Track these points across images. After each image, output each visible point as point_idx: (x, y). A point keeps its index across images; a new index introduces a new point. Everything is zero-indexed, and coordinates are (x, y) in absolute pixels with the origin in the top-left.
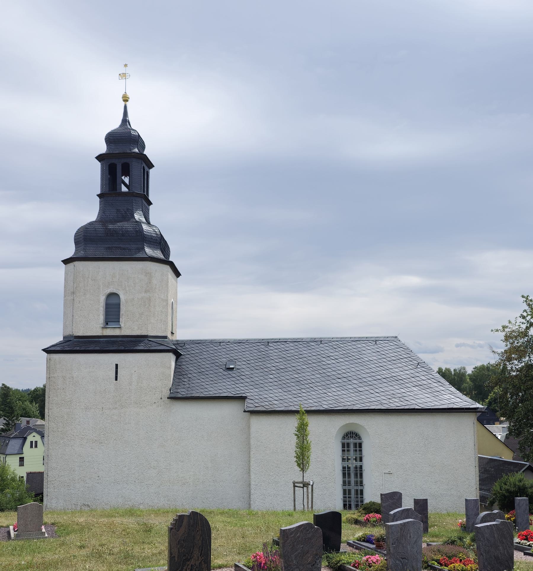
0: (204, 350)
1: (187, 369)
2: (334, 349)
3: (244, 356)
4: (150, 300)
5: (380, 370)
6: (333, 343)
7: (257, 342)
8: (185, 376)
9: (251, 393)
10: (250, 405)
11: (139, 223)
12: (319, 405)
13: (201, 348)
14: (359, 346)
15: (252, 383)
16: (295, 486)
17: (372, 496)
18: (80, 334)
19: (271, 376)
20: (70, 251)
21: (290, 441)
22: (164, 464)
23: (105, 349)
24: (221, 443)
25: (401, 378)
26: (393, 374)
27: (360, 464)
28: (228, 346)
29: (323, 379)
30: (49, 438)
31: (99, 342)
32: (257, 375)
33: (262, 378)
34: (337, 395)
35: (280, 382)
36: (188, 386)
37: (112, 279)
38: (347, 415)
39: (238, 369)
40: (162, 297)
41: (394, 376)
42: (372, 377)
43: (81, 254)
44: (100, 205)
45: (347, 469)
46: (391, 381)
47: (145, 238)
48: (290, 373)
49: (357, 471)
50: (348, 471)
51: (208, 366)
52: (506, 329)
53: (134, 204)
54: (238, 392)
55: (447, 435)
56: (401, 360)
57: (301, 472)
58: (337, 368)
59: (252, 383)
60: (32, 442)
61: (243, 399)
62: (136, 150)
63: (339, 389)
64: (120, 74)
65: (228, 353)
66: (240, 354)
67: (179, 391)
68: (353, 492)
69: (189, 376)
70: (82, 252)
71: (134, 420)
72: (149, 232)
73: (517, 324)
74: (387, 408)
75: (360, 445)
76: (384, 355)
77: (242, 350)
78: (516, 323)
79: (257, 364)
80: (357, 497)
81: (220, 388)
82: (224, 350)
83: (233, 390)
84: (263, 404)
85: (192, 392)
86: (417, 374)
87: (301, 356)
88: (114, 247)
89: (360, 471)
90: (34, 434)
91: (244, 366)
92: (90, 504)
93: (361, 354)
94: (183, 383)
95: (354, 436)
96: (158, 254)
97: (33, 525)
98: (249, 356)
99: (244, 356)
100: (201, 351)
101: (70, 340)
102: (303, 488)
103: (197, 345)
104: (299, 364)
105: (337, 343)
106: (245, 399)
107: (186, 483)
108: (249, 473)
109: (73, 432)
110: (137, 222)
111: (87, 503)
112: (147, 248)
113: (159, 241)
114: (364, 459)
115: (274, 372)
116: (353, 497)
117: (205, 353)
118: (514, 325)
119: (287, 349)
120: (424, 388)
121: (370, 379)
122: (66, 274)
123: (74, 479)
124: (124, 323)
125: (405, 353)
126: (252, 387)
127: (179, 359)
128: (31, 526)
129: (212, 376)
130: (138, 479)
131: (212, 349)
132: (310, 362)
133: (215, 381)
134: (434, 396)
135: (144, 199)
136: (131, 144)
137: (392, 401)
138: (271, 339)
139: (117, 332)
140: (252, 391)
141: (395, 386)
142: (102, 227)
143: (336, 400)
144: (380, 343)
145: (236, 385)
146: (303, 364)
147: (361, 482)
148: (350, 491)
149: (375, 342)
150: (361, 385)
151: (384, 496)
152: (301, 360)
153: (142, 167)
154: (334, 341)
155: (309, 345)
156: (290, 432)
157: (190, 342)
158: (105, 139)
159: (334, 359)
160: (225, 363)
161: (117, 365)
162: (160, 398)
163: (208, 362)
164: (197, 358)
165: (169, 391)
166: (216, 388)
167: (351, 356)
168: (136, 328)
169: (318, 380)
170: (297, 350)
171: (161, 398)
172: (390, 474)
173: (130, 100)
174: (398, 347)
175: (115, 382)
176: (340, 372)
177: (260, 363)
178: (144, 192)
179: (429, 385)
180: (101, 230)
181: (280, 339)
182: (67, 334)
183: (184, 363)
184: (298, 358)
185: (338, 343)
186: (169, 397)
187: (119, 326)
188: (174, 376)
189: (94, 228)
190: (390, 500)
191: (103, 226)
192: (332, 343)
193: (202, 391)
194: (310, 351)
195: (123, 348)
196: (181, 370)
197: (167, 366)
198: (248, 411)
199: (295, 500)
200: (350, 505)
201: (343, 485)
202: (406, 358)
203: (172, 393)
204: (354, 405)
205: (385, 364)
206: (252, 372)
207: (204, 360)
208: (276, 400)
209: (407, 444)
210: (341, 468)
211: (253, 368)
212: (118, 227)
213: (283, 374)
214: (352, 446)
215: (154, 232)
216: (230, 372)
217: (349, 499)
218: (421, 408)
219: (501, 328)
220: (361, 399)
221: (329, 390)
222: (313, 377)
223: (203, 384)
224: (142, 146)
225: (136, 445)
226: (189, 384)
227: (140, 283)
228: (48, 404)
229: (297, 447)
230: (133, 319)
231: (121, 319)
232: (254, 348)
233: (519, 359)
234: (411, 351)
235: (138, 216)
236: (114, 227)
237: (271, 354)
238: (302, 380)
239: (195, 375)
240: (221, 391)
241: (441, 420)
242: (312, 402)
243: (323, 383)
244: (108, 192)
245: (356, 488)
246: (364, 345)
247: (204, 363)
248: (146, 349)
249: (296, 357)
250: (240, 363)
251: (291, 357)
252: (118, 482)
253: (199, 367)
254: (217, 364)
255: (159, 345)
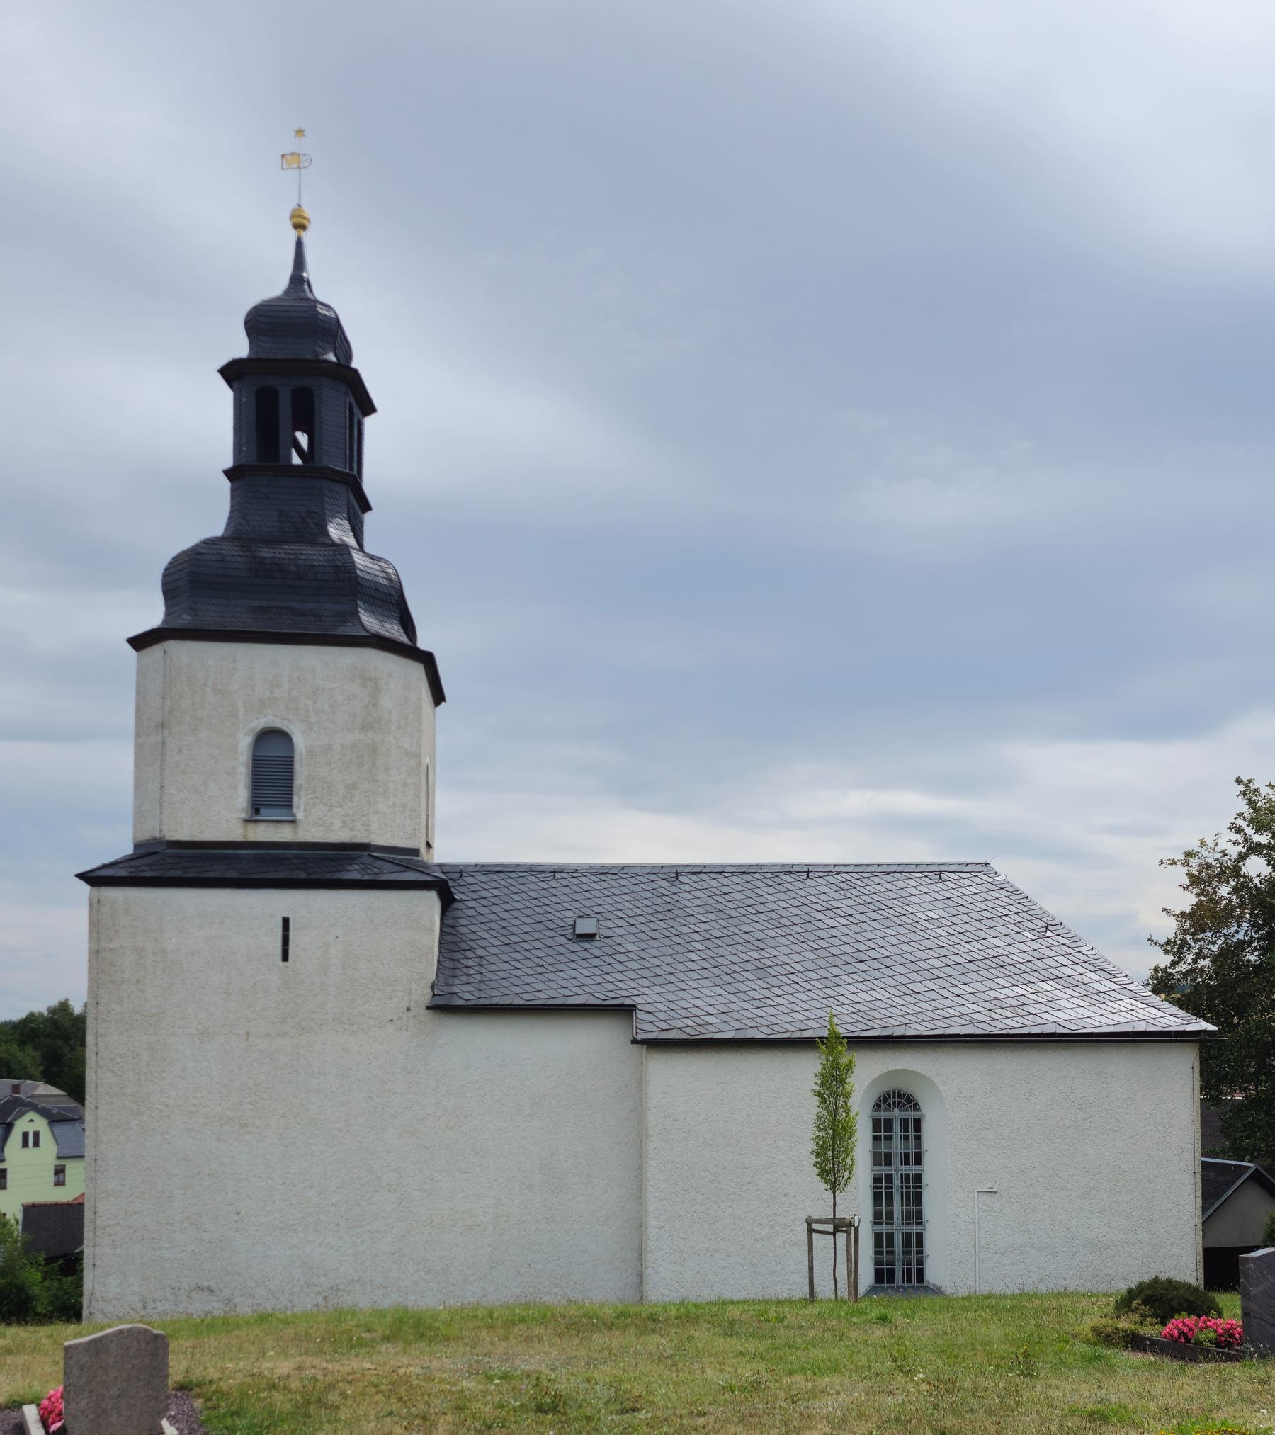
0: (513, 889)
1: (472, 936)
2: (842, 892)
3: (619, 906)
4: (375, 750)
5: (959, 941)
6: (837, 876)
7: (648, 873)
8: (469, 954)
9: (645, 997)
10: (648, 1027)
11: (344, 547)
12: (819, 1026)
13: (506, 885)
14: (901, 884)
15: (646, 973)
16: (811, 1231)
17: (949, 1248)
18: (183, 835)
19: (693, 956)
20: (153, 614)
21: (748, 1116)
22: (416, 1178)
23: (253, 876)
24: (568, 1124)
25: (1011, 962)
26: (990, 952)
27: (905, 1170)
28: (575, 881)
29: (822, 963)
30: (99, 1112)
31: (237, 857)
32: (655, 953)
33: (668, 960)
34: (860, 1000)
35: (716, 971)
36: (478, 977)
37: (272, 692)
38: (889, 1051)
39: (606, 937)
40: (406, 745)
41: (995, 957)
42: (942, 959)
43: (185, 620)
44: (233, 497)
45: (884, 1185)
46: (987, 967)
47: (359, 588)
48: (740, 947)
49: (909, 1187)
50: (886, 1188)
51: (527, 929)
52: (1191, 860)
53: (326, 506)
54: (613, 995)
55: (1130, 1098)
56: (1004, 917)
57: (830, 1193)
58: (855, 936)
59: (646, 973)
60: (25, 1135)
61: (626, 1010)
62: (331, 357)
63: (865, 988)
64: (283, 156)
65: (577, 897)
66: (609, 900)
67: (455, 989)
68: (898, 1240)
69: (480, 952)
70: (185, 616)
71: (334, 1065)
72: (370, 571)
73: (1218, 849)
74: (988, 1032)
75: (918, 1124)
76: (962, 905)
77: (612, 890)
78: (1216, 845)
79: (654, 926)
80: (909, 1253)
81: (565, 983)
82: (567, 890)
83: (598, 988)
84: (679, 1024)
85: (491, 993)
86: (1048, 952)
87: (761, 908)
88: (275, 607)
89: (917, 1187)
90: (32, 1115)
91: (620, 931)
92: (215, 1286)
93: (908, 903)
94: (465, 970)
95: (903, 1101)
96: (394, 631)
97: (129, 1414)
98: (631, 906)
99: (619, 906)
100: (506, 891)
101: (156, 853)
102: (834, 1234)
103: (494, 877)
104: (758, 926)
105: (846, 876)
106: (633, 1010)
107: (474, 1226)
108: (639, 1193)
109: (166, 1095)
110: (334, 544)
111: (206, 1284)
112: (364, 613)
113: (396, 598)
114: (926, 1159)
115: (698, 945)
116: (899, 1252)
117: (516, 897)
118: (1212, 851)
119: (726, 890)
120: (1068, 985)
121: (936, 963)
122: (141, 674)
123: (171, 1222)
124: (305, 810)
125: (1012, 902)
126: (646, 982)
127: (450, 909)
128: (120, 1416)
129: (539, 953)
130: (347, 1219)
131: (533, 886)
132: (787, 922)
133: (548, 967)
134: (1095, 1002)
135: (352, 490)
136: (318, 341)
137: (996, 1017)
138: (683, 865)
139: (284, 834)
140: (646, 991)
141: (999, 981)
142: (240, 553)
143: (860, 1014)
144: (950, 879)
145: (604, 976)
146: (770, 927)
147: (919, 1215)
148: (890, 1237)
149: (938, 876)
150: (915, 977)
151: (1255, 1264)
152: (762, 916)
153: (348, 404)
154: (838, 873)
155: (780, 881)
156: (748, 1093)
157: (476, 869)
158: (246, 323)
159: (843, 914)
160: (572, 923)
161: (286, 922)
162: (405, 1009)
163: (528, 920)
164: (495, 909)
165: (429, 990)
166: (553, 985)
167: (884, 907)
168: (338, 824)
169: (810, 965)
170: (750, 894)
171: (408, 1009)
172: (992, 1195)
173: (312, 228)
174: (995, 888)
175: (282, 964)
176: (861, 947)
177: (661, 923)
178: (351, 468)
179: (1079, 978)
180: (239, 559)
181: (705, 866)
182: (147, 834)
183: (463, 921)
184: (754, 912)
185: (850, 878)
186: (429, 1005)
187: (290, 818)
188: (440, 952)
189: (218, 554)
190: (1269, 1276)
191: (244, 549)
192: (836, 876)
193: (518, 990)
194: (783, 896)
195: (303, 875)
196: (457, 940)
197: (423, 925)
198: (643, 1042)
199: (811, 1268)
200: (891, 1273)
201: (875, 1223)
202: (1016, 913)
203: (438, 995)
204: (906, 1024)
205: (968, 927)
206: (643, 945)
207: (517, 914)
208: (711, 1014)
209: (1034, 1121)
210: (870, 1181)
211: (643, 937)
212: (285, 553)
213: (722, 951)
214: (896, 1127)
215: (384, 575)
216: (586, 945)
217: (890, 1257)
218: (1070, 1031)
219: (1182, 857)
220: (920, 1010)
221: (839, 989)
222: (797, 958)
223: (518, 973)
224: (345, 351)
225: (341, 1130)
226: (481, 973)
227: (347, 704)
228: (95, 1022)
229: (818, 1127)
230: (330, 800)
231: (295, 799)
232: (643, 886)
233: (1216, 931)
234: (1027, 897)
235: (338, 531)
236: (274, 553)
237: (686, 903)
238: (771, 964)
239: (494, 950)
240: (567, 992)
241: (1117, 1063)
242: (801, 1018)
243: (824, 973)
244: (255, 463)
245: (906, 1229)
246: (913, 883)
247: (516, 922)
248: (366, 878)
249: (750, 909)
250: (609, 924)
251: (739, 910)
252: (293, 1228)
253: (504, 932)
254: (551, 925)
255: (402, 869)
